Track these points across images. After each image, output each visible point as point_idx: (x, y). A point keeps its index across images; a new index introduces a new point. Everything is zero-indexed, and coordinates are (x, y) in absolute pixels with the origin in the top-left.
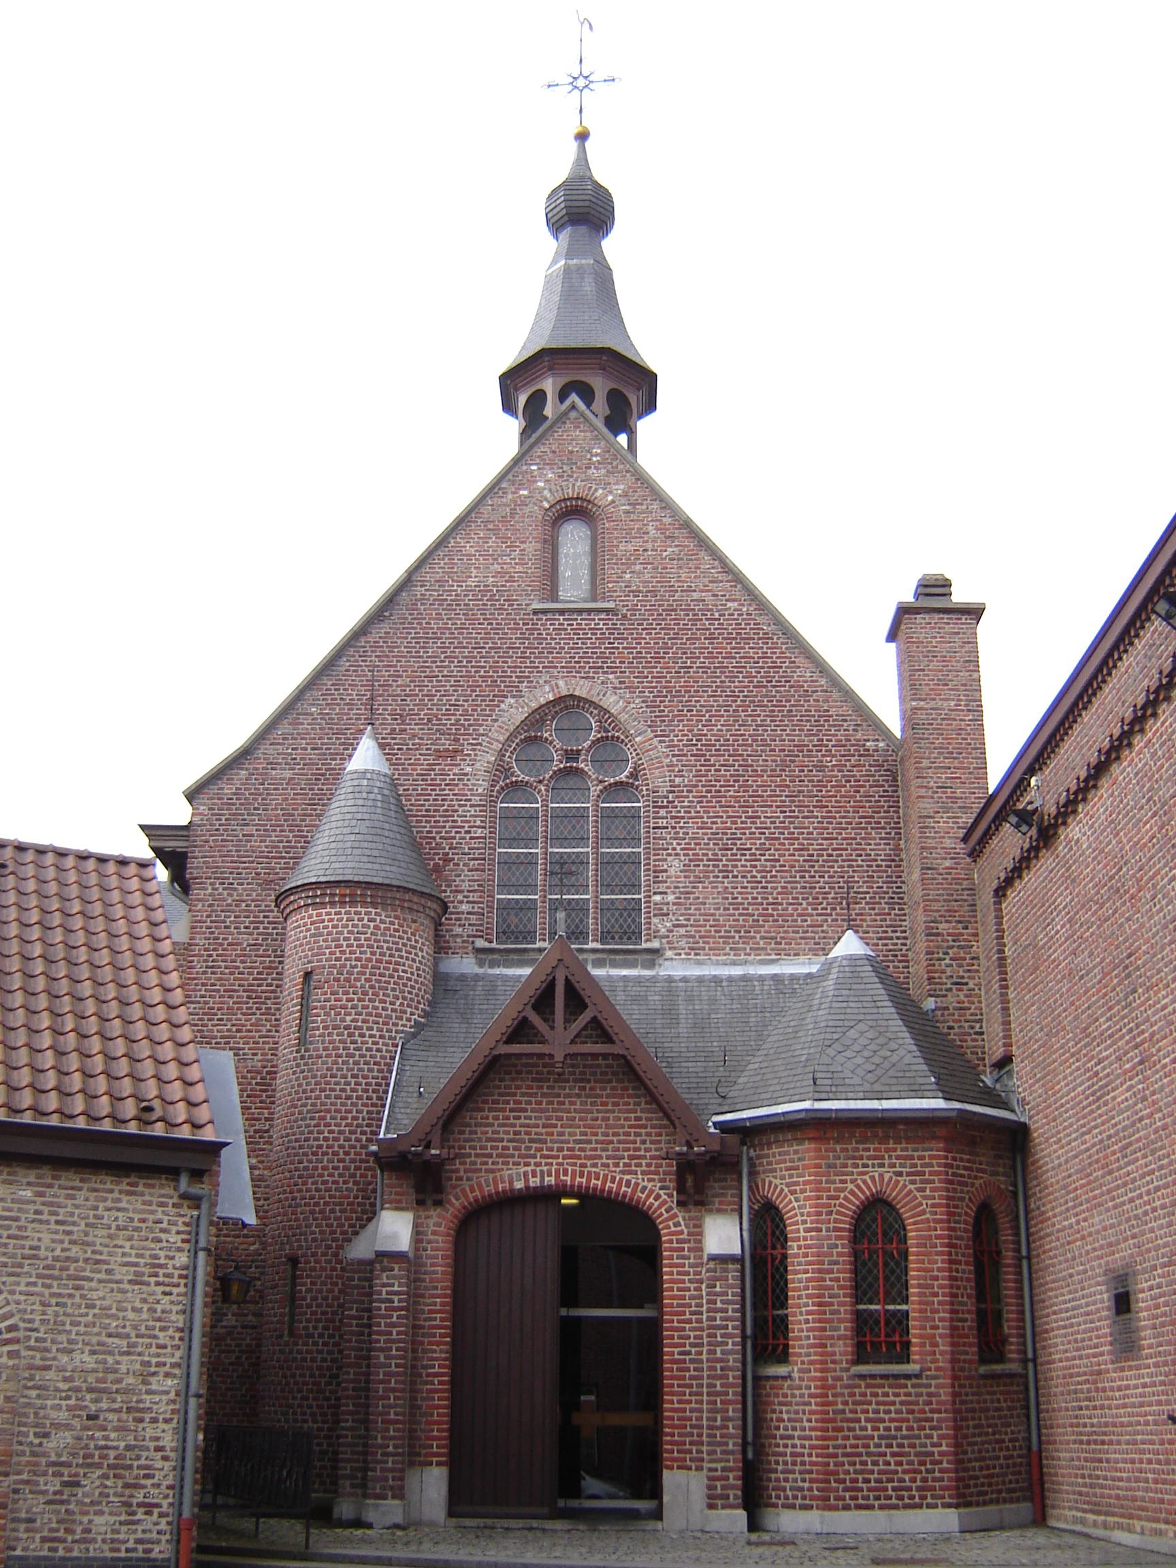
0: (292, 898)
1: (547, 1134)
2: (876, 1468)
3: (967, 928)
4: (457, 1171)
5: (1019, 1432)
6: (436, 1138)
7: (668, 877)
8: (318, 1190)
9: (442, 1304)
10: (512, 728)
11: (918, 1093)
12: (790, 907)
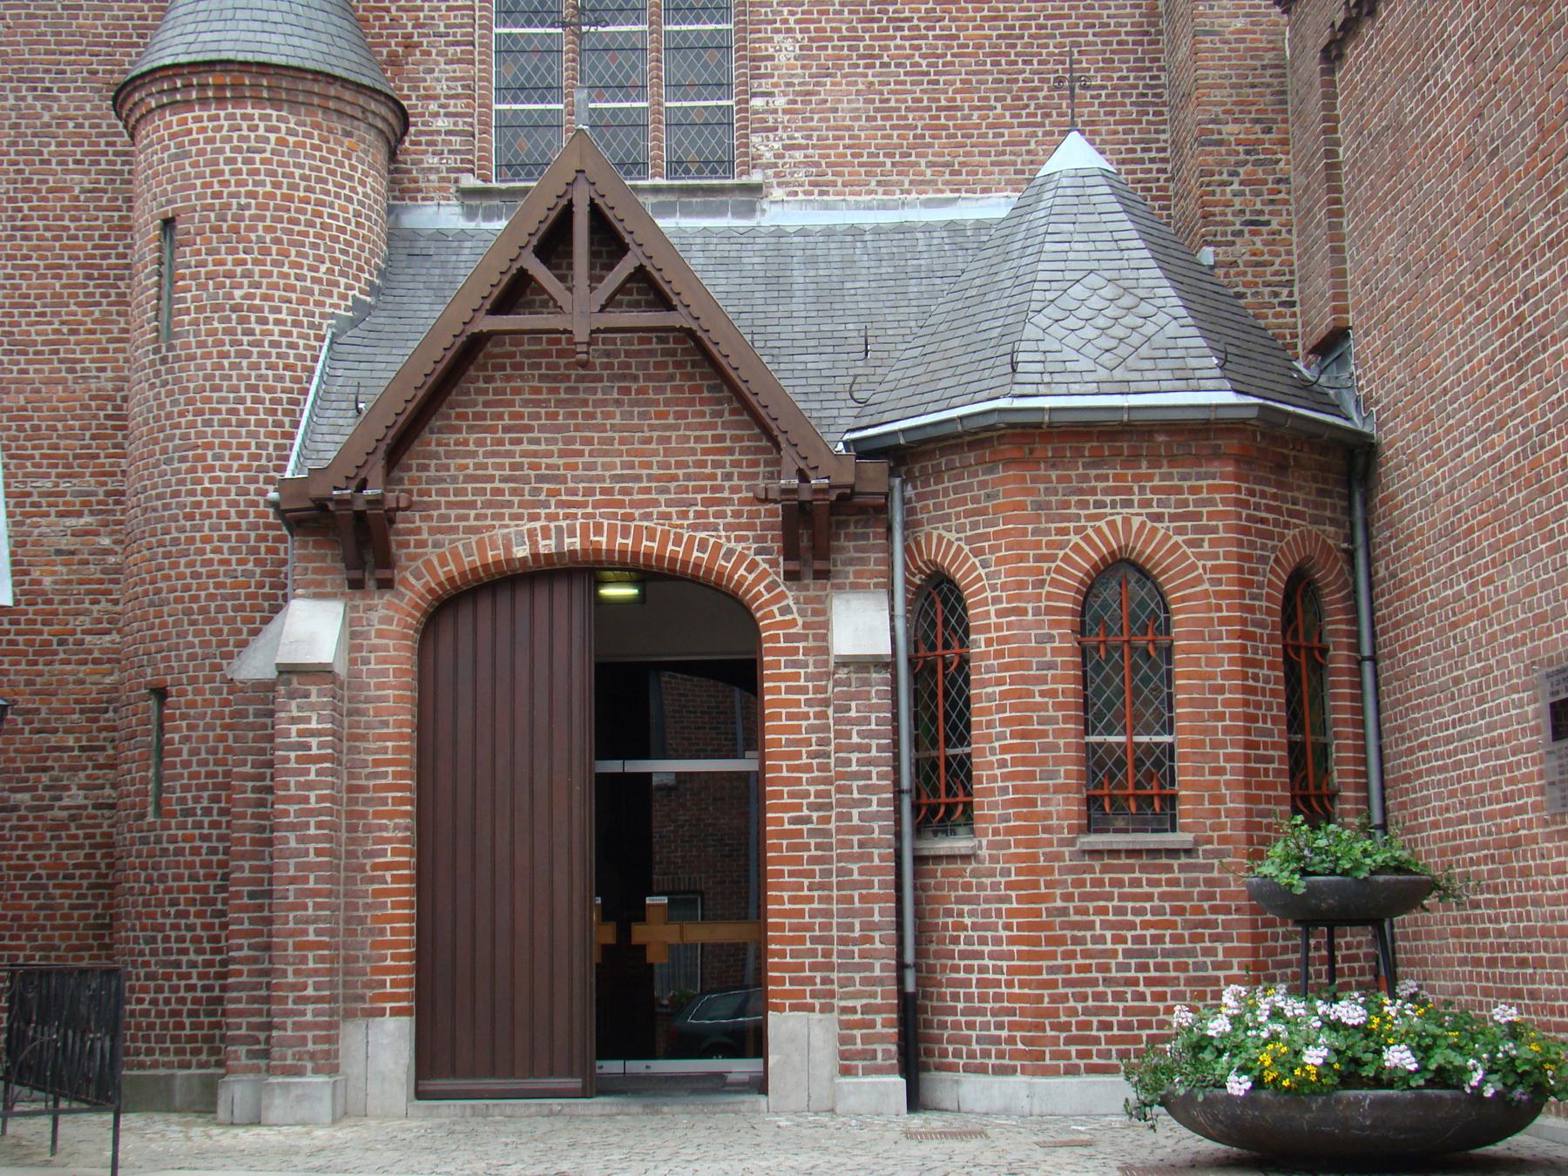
0: (137, 96)
1: (567, 467)
2: (1121, 1005)
3: (1268, 131)
4: (418, 531)
5: (1359, 945)
6: (376, 473)
7: (776, 68)
9: (397, 750)
11: (1187, 380)
12: (976, 114)
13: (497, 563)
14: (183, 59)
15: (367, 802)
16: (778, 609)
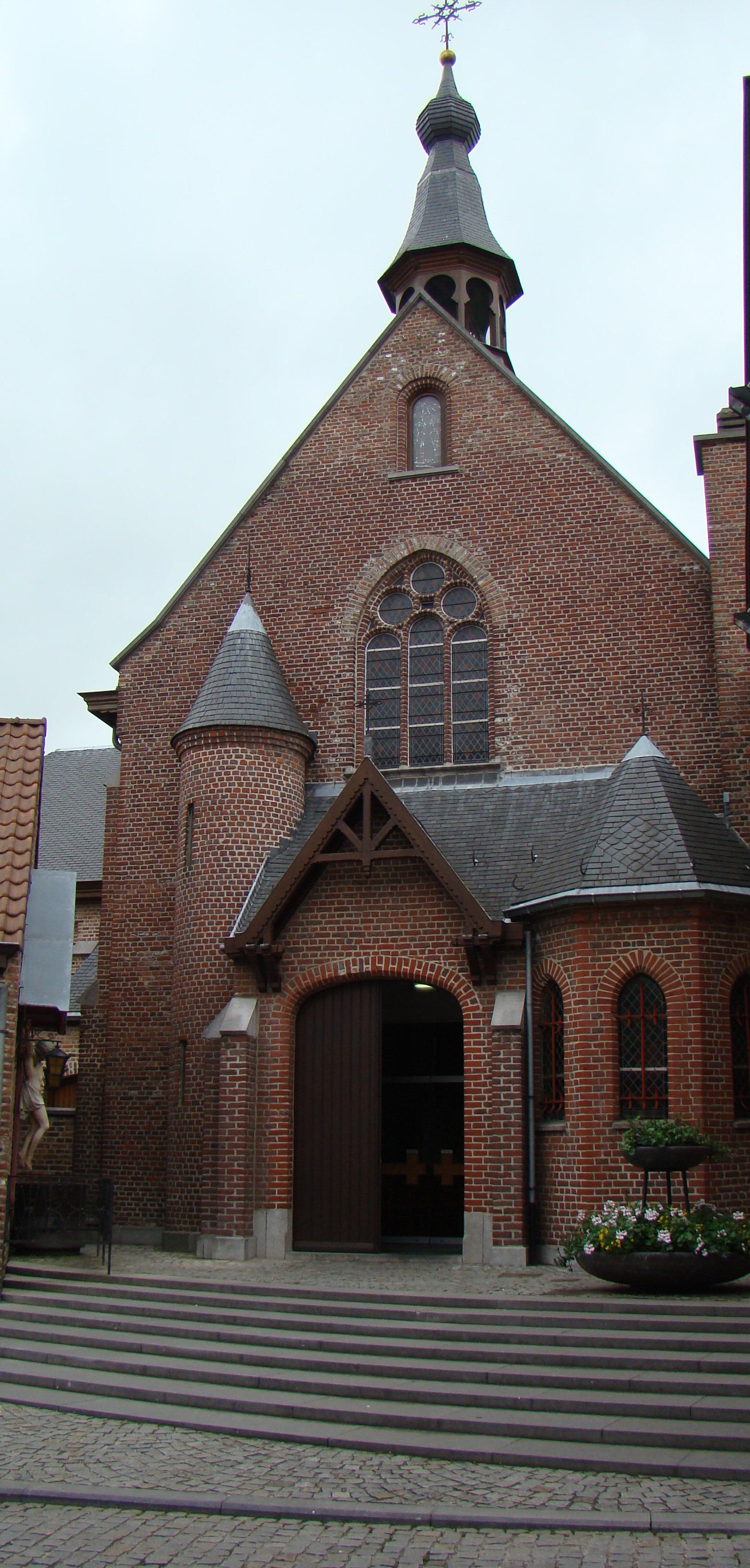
4: (292, 962)
6: (267, 936)
8: (200, 983)
9: (282, 1074)
10: (373, 584)
11: (675, 877)
12: (615, 720)
13: (331, 978)
14: (197, 725)
15: (267, 1100)
16: (470, 1000)
